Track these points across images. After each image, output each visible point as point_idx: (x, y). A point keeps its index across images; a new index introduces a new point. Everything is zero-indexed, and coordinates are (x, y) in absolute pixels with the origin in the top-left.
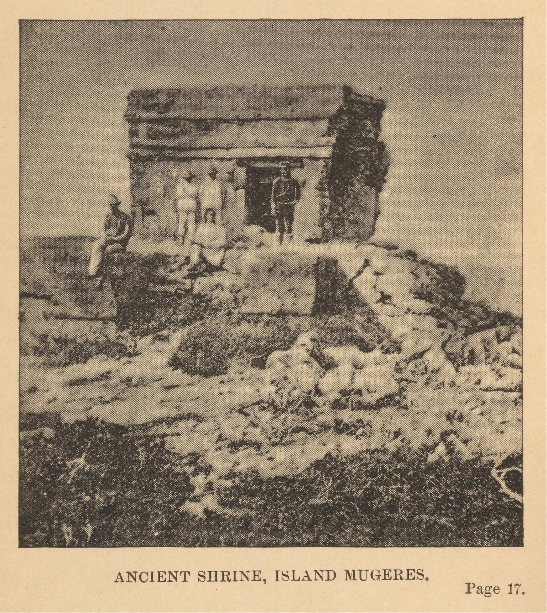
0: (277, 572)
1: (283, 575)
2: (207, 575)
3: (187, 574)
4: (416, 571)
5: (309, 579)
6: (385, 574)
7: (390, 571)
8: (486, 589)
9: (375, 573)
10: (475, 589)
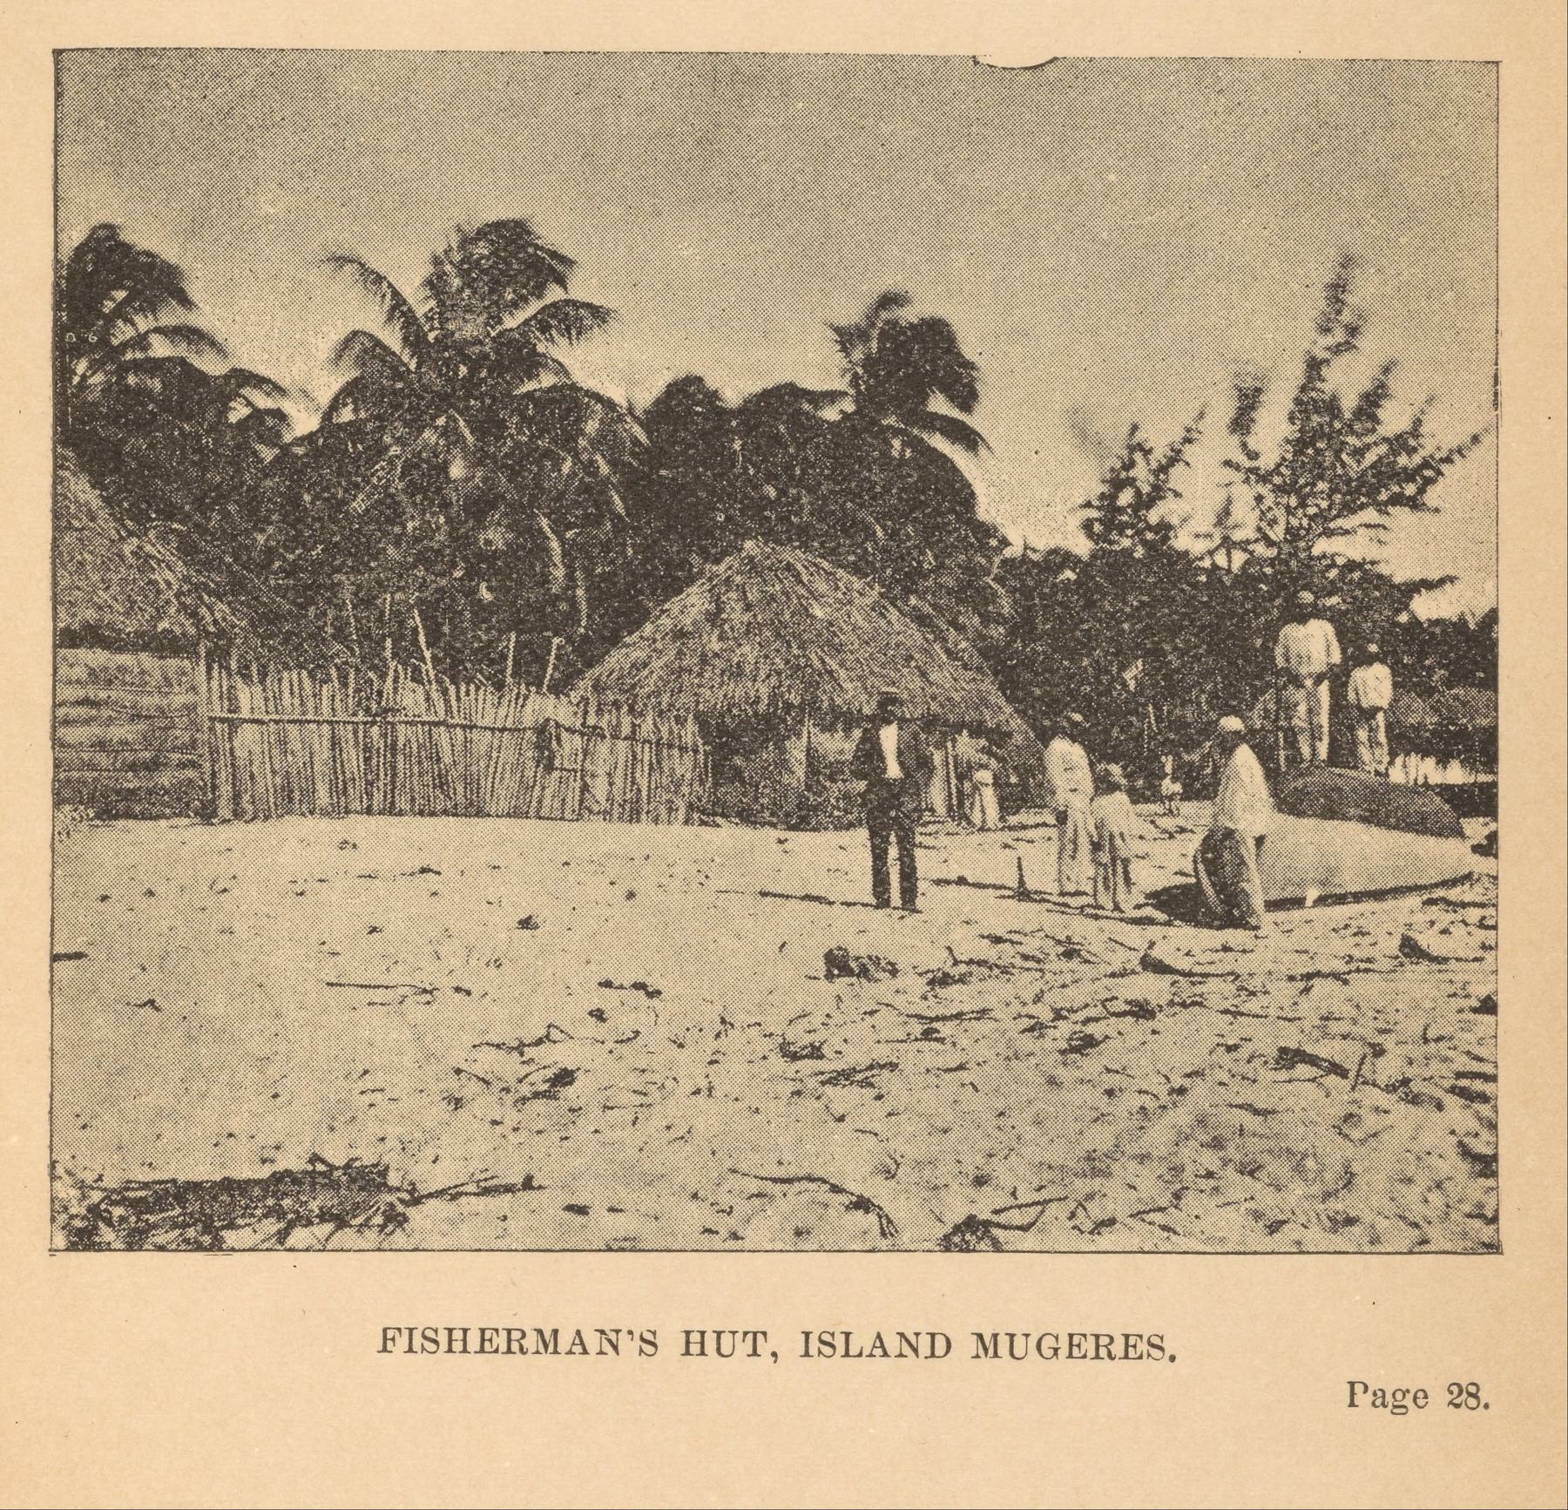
0: (807, 1335)
1: (425, 1338)
2: (443, 1338)
3: (760, 1336)
4: (1145, 1339)
5: (885, 1354)
6: (1071, 1345)
7: (1085, 1336)
8: (1394, 1394)
9: (1048, 1343)
10: (1369, 1397)
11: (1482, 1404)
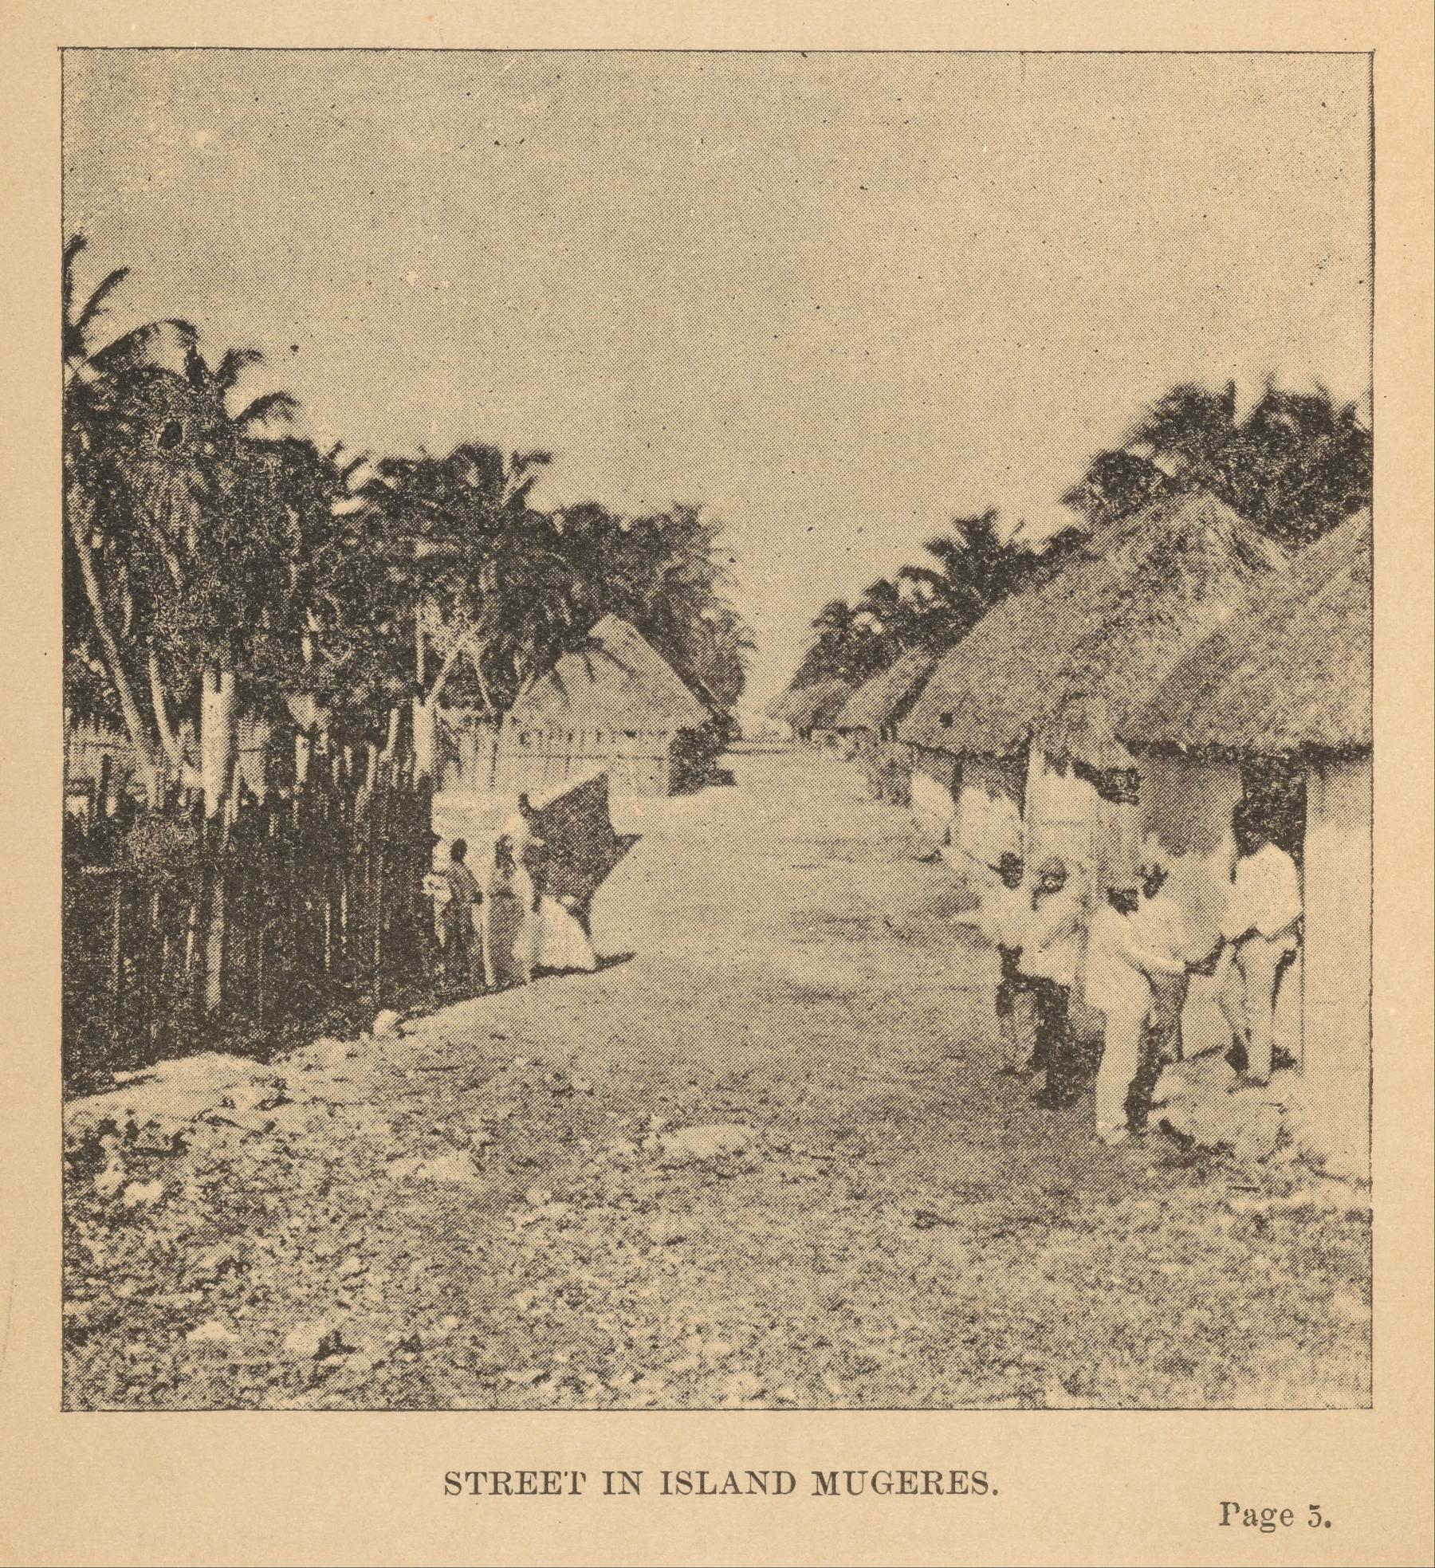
0: (666, 1474)
3: (481, 1476)
4: (970, 1475)
5: (737, 1492)
7: (535, 1474)
9: (882, 1479)
10: (1241, 1516)
11: (1323, 1521)
